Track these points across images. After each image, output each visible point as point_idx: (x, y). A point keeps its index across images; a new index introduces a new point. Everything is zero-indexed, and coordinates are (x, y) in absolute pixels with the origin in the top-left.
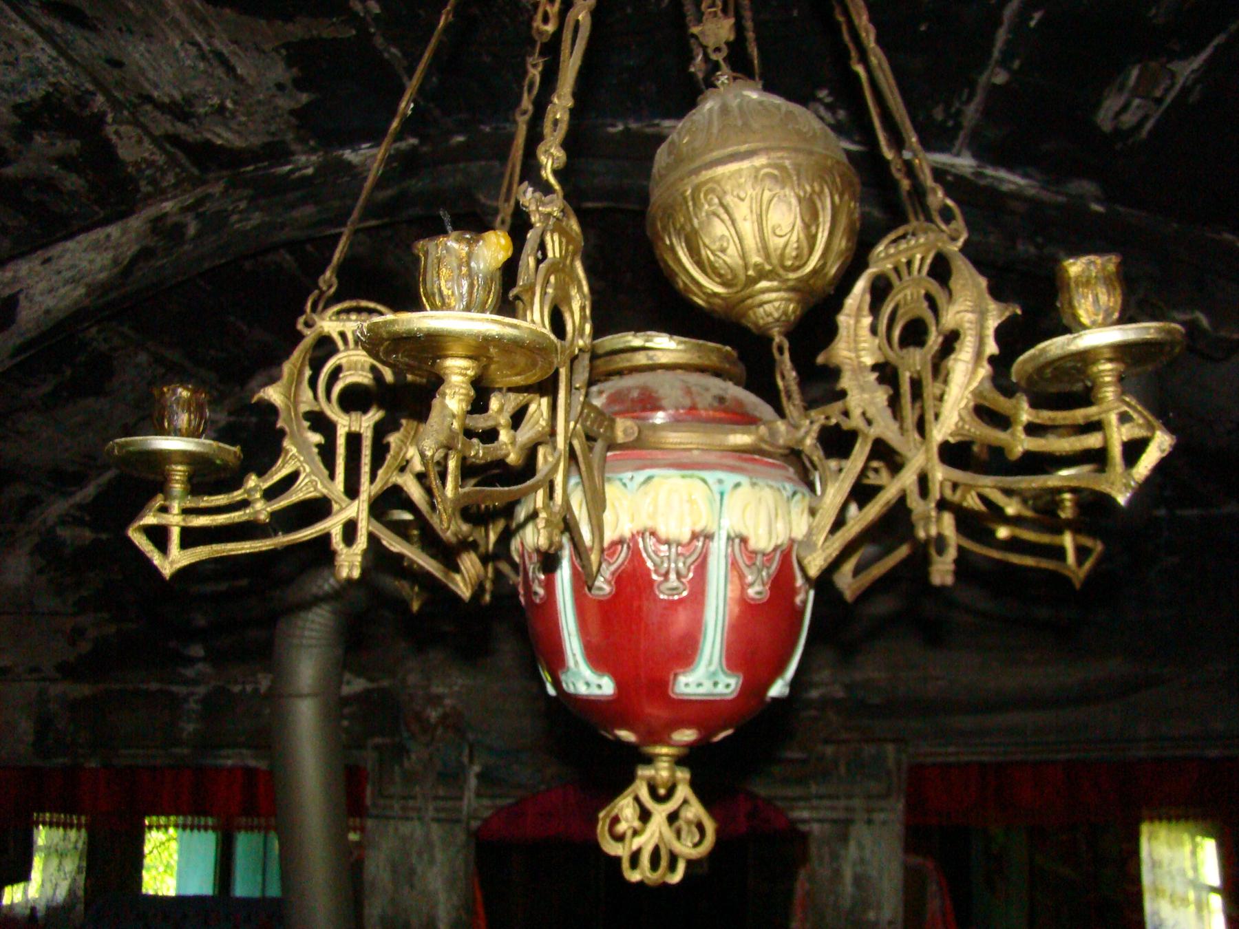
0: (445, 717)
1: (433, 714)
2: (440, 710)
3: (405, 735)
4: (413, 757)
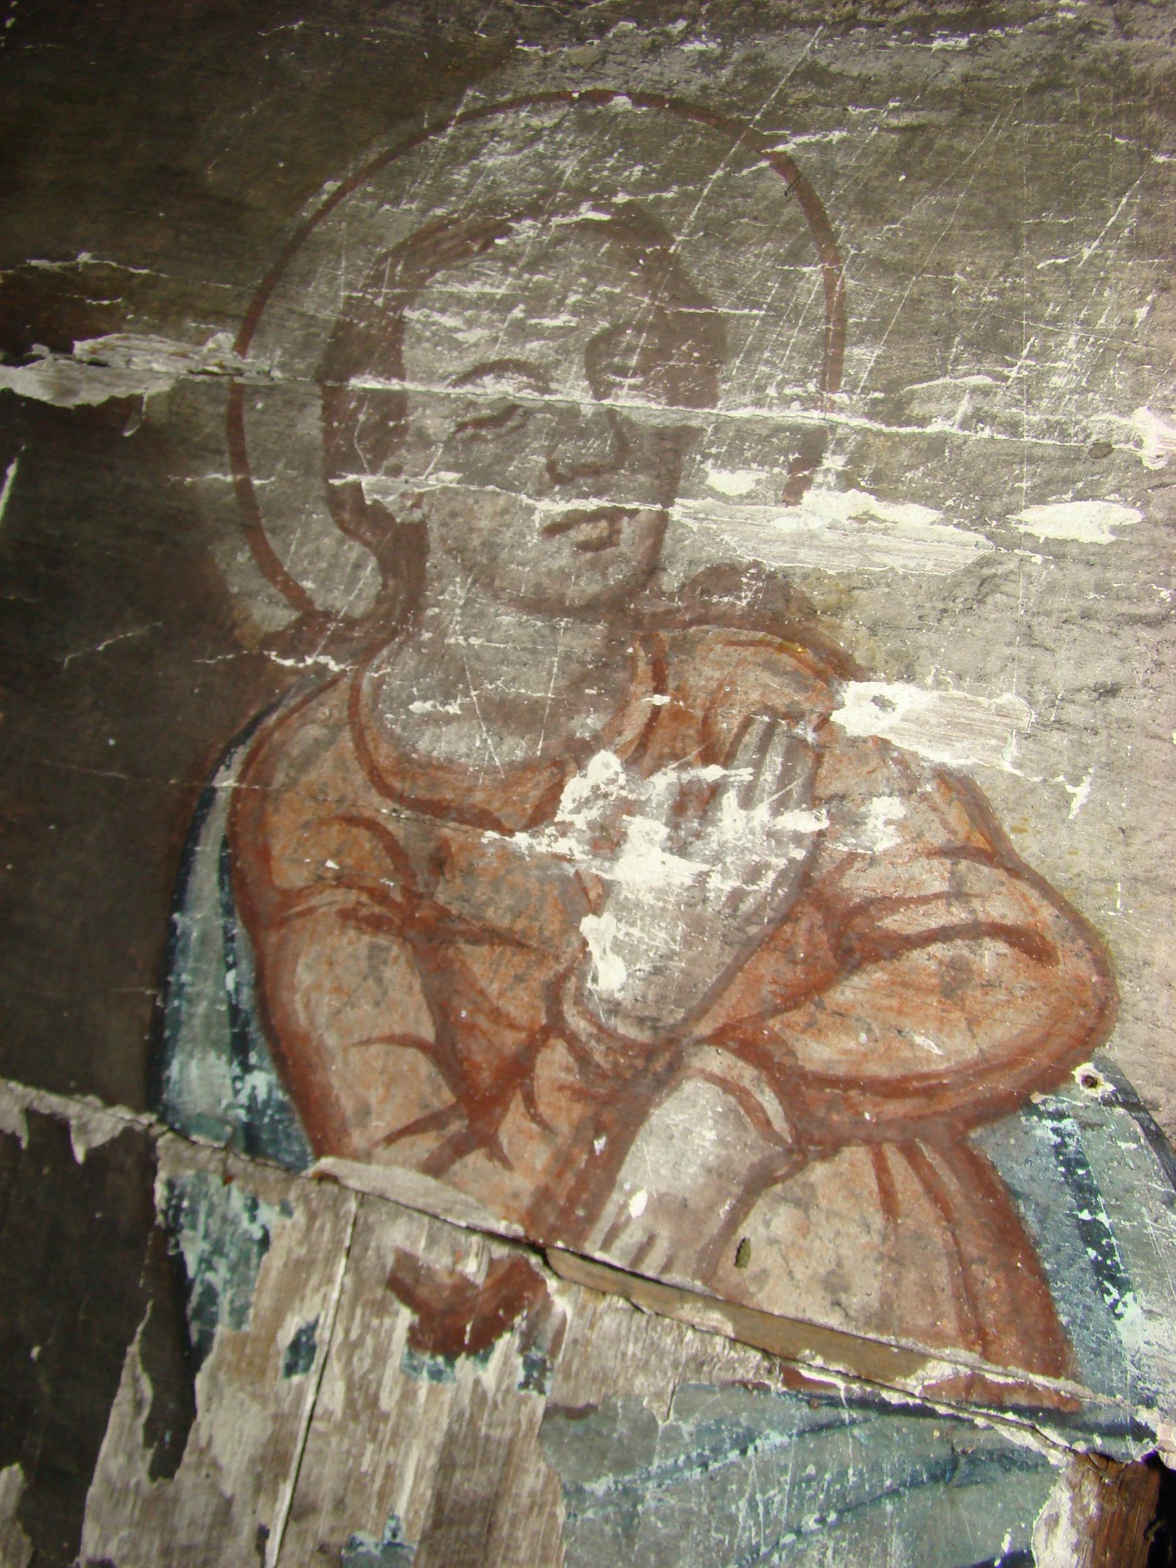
0: (824, 929)
1: (646, 878)
2: (757, 830)
3: (202, 1077)
4: (229, 1424)
